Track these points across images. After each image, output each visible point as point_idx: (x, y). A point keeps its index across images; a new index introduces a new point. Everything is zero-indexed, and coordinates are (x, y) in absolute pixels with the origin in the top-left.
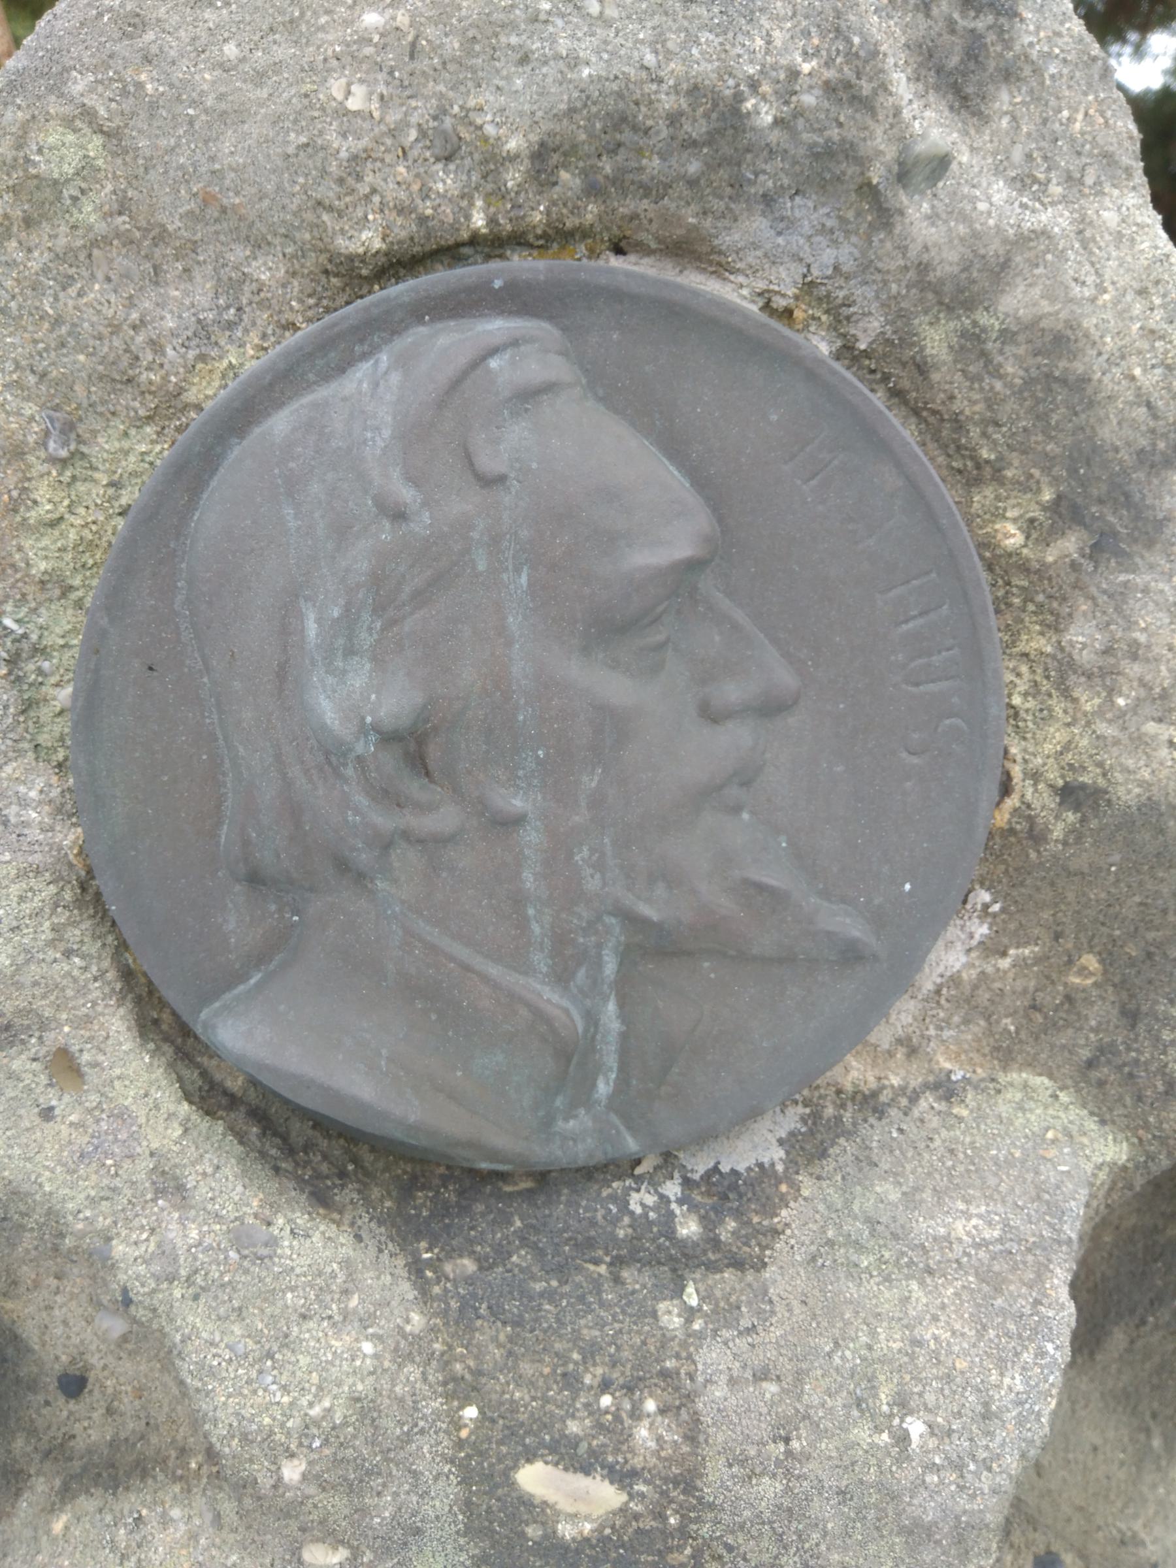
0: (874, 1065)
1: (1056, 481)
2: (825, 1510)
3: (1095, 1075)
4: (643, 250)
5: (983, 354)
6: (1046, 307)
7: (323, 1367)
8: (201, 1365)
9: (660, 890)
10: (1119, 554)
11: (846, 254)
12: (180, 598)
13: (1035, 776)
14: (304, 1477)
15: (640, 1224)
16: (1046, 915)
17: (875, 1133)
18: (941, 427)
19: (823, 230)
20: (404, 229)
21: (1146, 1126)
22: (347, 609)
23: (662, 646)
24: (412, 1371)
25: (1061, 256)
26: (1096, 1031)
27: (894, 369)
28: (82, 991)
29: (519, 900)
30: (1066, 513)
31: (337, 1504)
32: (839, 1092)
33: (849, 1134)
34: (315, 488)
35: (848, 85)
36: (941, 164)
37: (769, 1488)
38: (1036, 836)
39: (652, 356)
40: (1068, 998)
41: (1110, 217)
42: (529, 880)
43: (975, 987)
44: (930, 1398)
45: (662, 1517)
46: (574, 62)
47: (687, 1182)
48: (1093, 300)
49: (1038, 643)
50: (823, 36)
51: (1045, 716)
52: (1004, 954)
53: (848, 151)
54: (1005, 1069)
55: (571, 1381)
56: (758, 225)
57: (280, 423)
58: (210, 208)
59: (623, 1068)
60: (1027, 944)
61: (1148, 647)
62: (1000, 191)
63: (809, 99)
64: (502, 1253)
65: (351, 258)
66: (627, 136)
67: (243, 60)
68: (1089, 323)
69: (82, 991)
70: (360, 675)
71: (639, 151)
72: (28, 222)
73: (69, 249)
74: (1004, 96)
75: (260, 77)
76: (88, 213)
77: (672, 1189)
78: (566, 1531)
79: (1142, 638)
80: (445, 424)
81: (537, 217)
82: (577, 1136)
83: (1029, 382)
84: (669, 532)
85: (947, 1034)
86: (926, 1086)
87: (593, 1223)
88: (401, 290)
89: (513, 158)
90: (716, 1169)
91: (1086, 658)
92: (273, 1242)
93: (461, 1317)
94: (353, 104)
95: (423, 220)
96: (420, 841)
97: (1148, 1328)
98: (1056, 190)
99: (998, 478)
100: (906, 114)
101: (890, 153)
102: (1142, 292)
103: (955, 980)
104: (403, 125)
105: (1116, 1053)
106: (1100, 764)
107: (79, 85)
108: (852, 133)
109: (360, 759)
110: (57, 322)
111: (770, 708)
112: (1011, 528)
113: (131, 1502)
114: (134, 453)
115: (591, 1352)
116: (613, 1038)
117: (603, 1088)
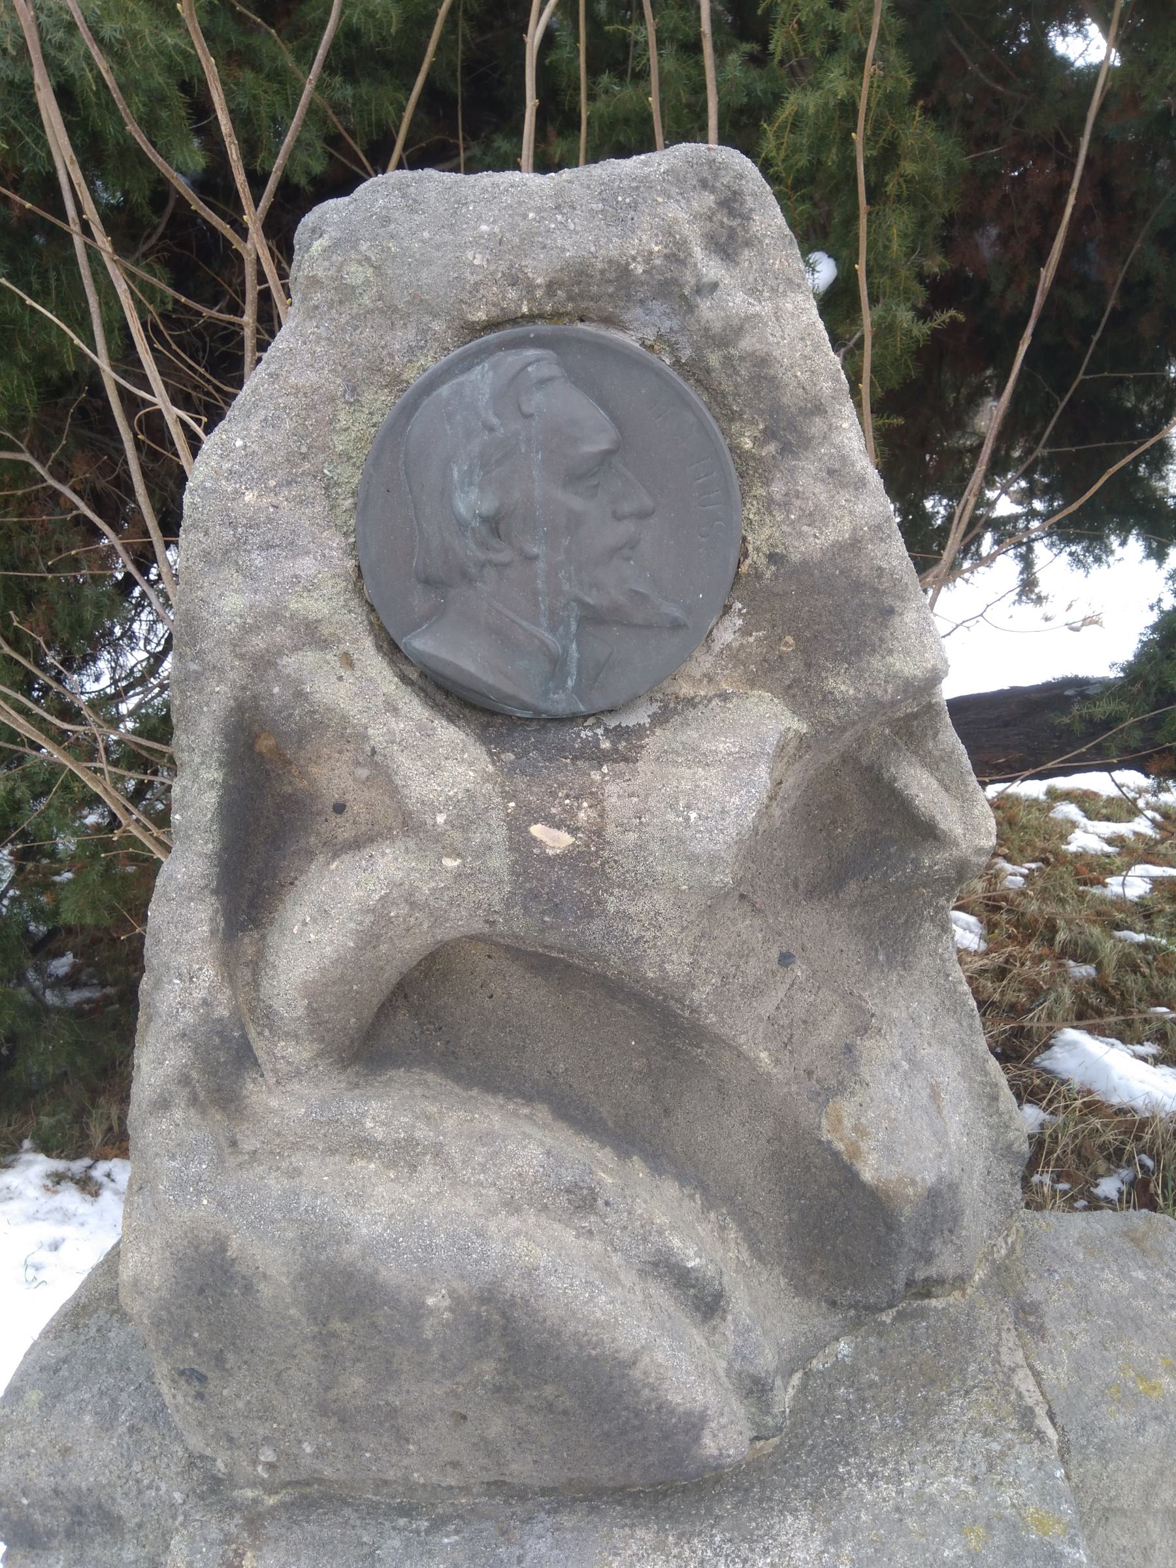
0: (694, 686)
1: (765, 420)
2: (654, 846)
3: (791, 692)
4: (592, 320)
5: (733, 366)
6: (758, 346)
7: (454, 777)
8: (405, 776)
9: (594, 592)
10: (792, 452)
11: (675, 323)
12: (400, 462)
13: (758, 549)
14: (445, 823)
15: (585, 742)
16: (768, 616)
17: (691, 714)
18: (717, 397)
19: (665, 314)
21: (815, 717)
22: (470, 467)
23: (596, 486)
24: (489, 786)
25: (766, 324)
26: (793, 672)
27: (695, 371)
28: (355, 628)
29: (535, 593)
30: (769, 434)
31: (457, 835)
32: (677, 698)
33: (679, 714)
34: (458, 417)
35: (674, 255)
36: (715, 286)
37: (632, 837)
38: (759, 576)
39: (593, 366)
40: (780, 657)
41: (789, 306)
42: (540, 584)
43: (739, 650)
44: (700, 805)
45: (588, 846)
46: (563, 250)
47: (606, 730)
48: (778, 343)
49: (762, 492)
50: (663, 236)
51: (762, 524)
52: (751, 635)
53: (675, 282)
54: (751, 689)
55: (553, 794)
56: (638, 311)
57: (445, 390)
58: (417, 301)
59: (579, 674)
60: (760, 630)
61: (804, 493)
62: (740, 296)
63: (658, 262)
64: (526, 752)
65: (473, 323)
66: (584, 278)
67: (431, 239)
69: (355, 628)
70: (474, 495)
71: (589, 285)
72: (341, 302)
73: (357, 314)
74: (746, 253)
75: (438, 247)
76: (366, 300)
77: (600, 731)
78: (550, 852)
79: (801, 489)
80: (510, 393)
81: (548, 308)
82: (559, 702)
83: (752, 378)
85: (726, 672)
86: (716, 695)
87: (565, 741)
88: (492, 337)
89: (539, 286)
90: (619, 726)
91: (778, 497)
92: (434, 729)
93: (510, 771)
94: (476, 262)
95: (502, 309)
96: (496, 565)
97: (869, 881)
98: (766, 294)
99: (741, 418)
100: (699, 265)
101: (693, 281)
102: (802, 339)
103: (729, 646)
104: (496, 271)
105: (801, 682)
106: (784, 544)
107: (364, 246)
108: (676, 274)
109: (473, 529)
110: (351, 345)
111: (642, 515)
112: (747, 440)
113: (366, 852)
114: (380, 400)
115: (562, 785)
116: (574, 660)
117: (570, 683)
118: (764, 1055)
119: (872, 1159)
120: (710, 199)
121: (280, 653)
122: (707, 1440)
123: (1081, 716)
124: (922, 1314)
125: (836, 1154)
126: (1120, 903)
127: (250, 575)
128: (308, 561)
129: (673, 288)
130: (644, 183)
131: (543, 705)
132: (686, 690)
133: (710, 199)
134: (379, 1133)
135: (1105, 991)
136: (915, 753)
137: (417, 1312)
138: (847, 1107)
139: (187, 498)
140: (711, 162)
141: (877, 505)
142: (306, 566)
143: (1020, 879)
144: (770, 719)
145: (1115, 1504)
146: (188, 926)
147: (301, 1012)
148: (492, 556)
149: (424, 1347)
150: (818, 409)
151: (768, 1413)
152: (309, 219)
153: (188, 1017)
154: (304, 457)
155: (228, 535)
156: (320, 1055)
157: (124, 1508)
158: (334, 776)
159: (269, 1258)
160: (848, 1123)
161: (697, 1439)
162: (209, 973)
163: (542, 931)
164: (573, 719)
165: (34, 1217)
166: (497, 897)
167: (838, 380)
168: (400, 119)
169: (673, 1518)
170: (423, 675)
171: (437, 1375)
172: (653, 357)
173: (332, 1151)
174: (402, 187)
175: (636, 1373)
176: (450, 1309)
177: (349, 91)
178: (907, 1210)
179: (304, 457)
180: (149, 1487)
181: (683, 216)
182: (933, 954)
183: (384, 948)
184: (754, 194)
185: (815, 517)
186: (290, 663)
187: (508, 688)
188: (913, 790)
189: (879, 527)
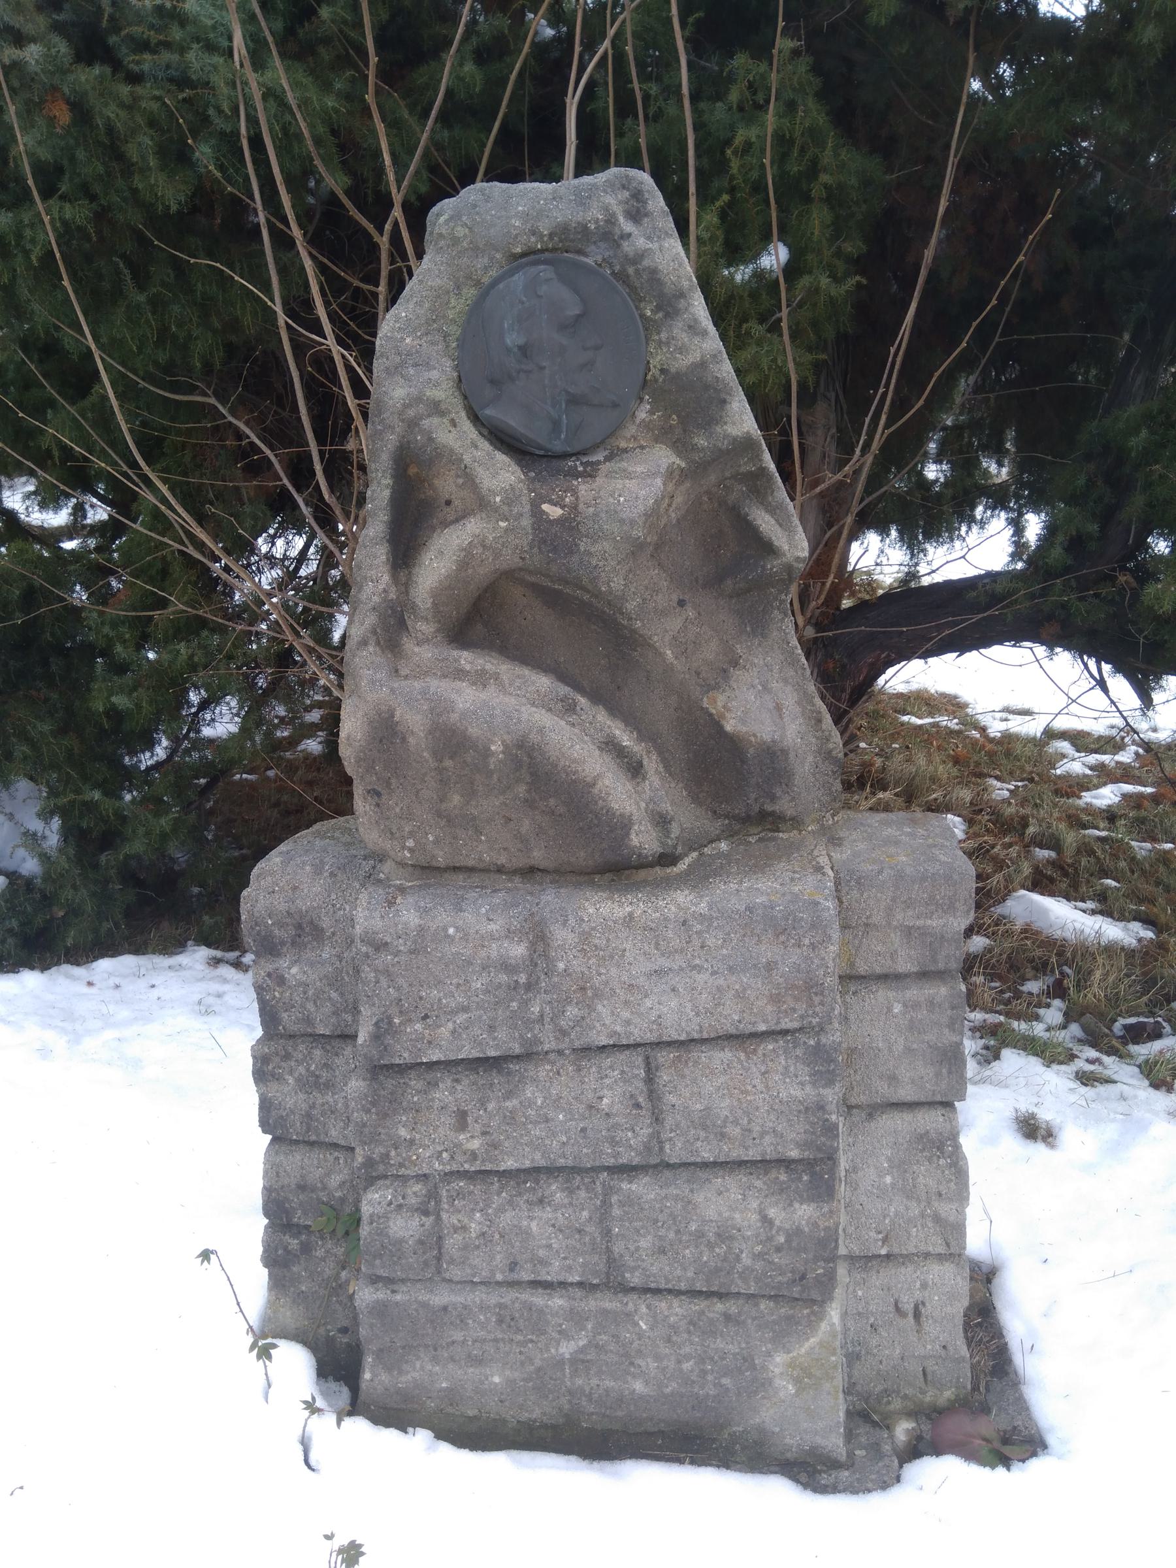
11: (611, 253)
18: (633, 290)
20: (525, 248)
27: (622, 277)
31: (506, 508)
36: (630, 235)
37: (591, 510)
38: (656, 381)
42: (546, 382)
49: (657, 337)
56: (593, 247)
57: (501, 286)
62: (642, 240)
68: (660, 267)
76: (465, 244)
82: (558, 446)
84: (574, 310)
93: (532, 480)
107: (464, 218)
114: (470, 293)
115: (557, 486)
117: (563, 437)
118: (669, 652)
119: (732, 722)
120: (627, 194)
121: (421, 419)
122: (633, 836)
123: (985, 591)
124: (774, 839)
125: (711, 715)
126: (1089, 809)
127: (407, 379)
128: (435, 372)
129: (609, 235)
130: (594, 186)
131: (549, 446)
132: (623, 444)
133: (627, 194)
134: (468, 667)
135: (1062, 868)
136: (762, 503)
137: (486, 753)
138: (721, 699)
139: (378, 342)
140: (627, 176)
141: (713, 342)
142: (434, 374)
143: (1006, 792)
144: (664, 457)
145: (870, 921)
146: (375, 557)
147: (429, 605)
148: (523, 366)
149: (489, 774)
150: (681, 295)
151: (668, 837)
152: (435, 210)
153: (376, 599)
154: (434, 321)
155: (398, 359)
156: (438, 631)
157: (326, 923)
158: (447, 485)
159: (414, 721)
160: (720, 704)
161: (628, 834)
162: (386, 578)
163: (548, 563)
164: (566, 456)
165: (202, 979)
166: (525, 543)
167: (691, 281)
168: (483, 152)
169: (618, 890)
170: (491, 433)
171: (496, 791)
172: (601, 270)
173: (445, 677)
174: (482, 191)
175: (596, 791)
176: (503, 752)
177: (446, 134)
178: (751, 751)
179: (434, 321)
180: (340, 909)
181: (613, 202)
182: (780, 629)
183: (470, 571)
184: (648, 191)
185: (682, 350)
186: (426, 423)
187: (531, 435)
188: (759, 522)
189: (715, 356)
